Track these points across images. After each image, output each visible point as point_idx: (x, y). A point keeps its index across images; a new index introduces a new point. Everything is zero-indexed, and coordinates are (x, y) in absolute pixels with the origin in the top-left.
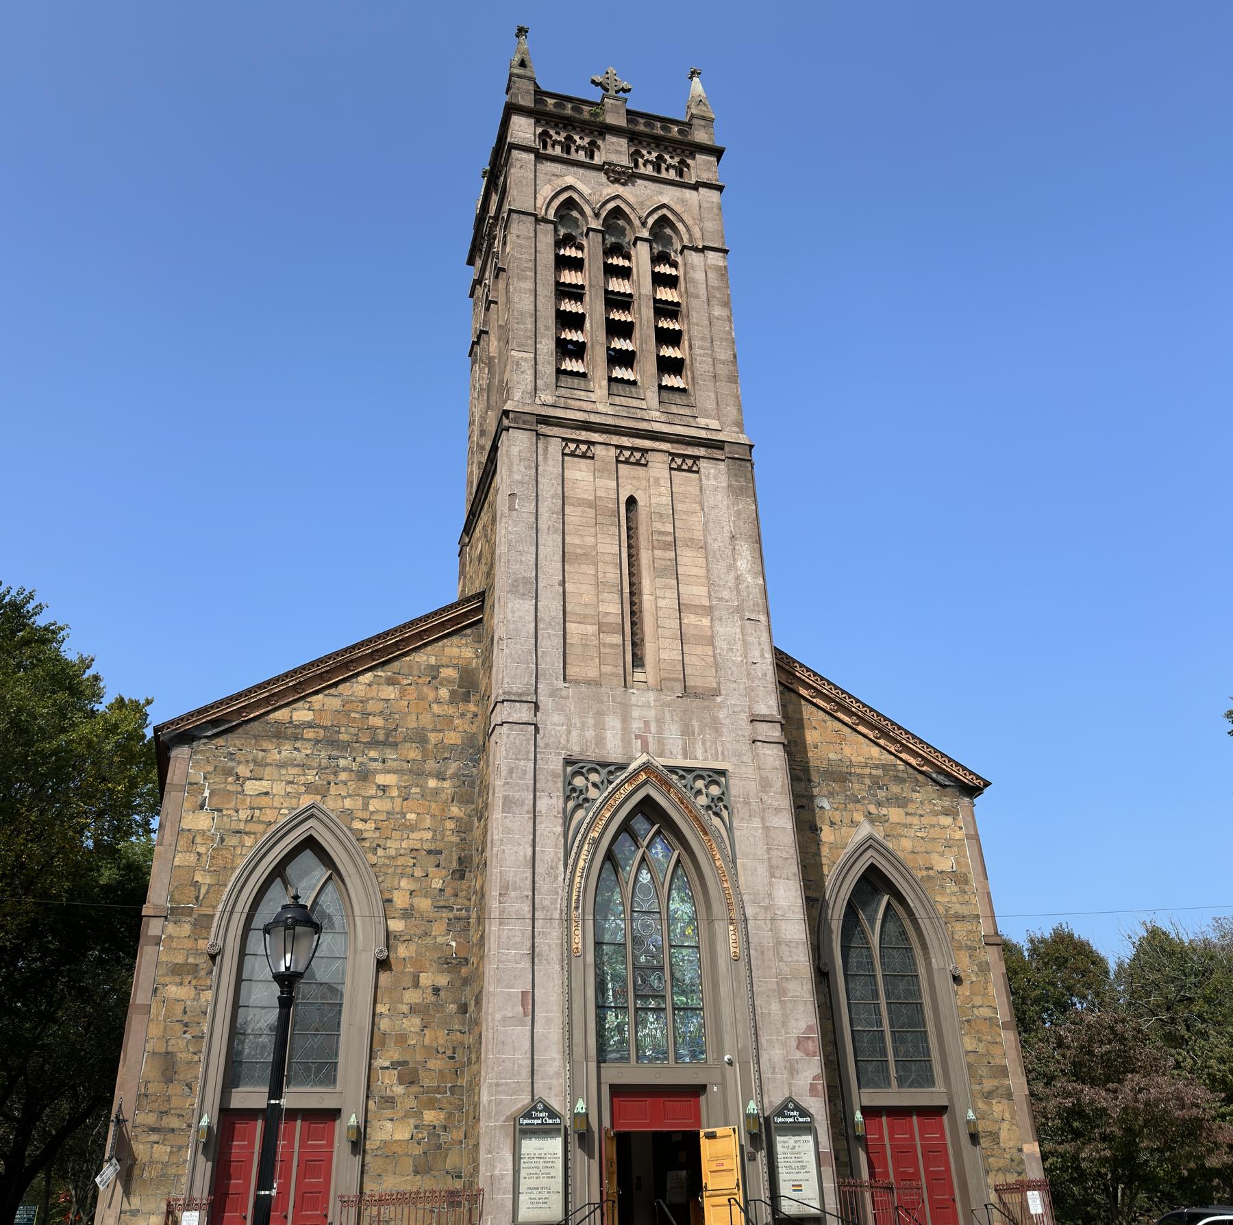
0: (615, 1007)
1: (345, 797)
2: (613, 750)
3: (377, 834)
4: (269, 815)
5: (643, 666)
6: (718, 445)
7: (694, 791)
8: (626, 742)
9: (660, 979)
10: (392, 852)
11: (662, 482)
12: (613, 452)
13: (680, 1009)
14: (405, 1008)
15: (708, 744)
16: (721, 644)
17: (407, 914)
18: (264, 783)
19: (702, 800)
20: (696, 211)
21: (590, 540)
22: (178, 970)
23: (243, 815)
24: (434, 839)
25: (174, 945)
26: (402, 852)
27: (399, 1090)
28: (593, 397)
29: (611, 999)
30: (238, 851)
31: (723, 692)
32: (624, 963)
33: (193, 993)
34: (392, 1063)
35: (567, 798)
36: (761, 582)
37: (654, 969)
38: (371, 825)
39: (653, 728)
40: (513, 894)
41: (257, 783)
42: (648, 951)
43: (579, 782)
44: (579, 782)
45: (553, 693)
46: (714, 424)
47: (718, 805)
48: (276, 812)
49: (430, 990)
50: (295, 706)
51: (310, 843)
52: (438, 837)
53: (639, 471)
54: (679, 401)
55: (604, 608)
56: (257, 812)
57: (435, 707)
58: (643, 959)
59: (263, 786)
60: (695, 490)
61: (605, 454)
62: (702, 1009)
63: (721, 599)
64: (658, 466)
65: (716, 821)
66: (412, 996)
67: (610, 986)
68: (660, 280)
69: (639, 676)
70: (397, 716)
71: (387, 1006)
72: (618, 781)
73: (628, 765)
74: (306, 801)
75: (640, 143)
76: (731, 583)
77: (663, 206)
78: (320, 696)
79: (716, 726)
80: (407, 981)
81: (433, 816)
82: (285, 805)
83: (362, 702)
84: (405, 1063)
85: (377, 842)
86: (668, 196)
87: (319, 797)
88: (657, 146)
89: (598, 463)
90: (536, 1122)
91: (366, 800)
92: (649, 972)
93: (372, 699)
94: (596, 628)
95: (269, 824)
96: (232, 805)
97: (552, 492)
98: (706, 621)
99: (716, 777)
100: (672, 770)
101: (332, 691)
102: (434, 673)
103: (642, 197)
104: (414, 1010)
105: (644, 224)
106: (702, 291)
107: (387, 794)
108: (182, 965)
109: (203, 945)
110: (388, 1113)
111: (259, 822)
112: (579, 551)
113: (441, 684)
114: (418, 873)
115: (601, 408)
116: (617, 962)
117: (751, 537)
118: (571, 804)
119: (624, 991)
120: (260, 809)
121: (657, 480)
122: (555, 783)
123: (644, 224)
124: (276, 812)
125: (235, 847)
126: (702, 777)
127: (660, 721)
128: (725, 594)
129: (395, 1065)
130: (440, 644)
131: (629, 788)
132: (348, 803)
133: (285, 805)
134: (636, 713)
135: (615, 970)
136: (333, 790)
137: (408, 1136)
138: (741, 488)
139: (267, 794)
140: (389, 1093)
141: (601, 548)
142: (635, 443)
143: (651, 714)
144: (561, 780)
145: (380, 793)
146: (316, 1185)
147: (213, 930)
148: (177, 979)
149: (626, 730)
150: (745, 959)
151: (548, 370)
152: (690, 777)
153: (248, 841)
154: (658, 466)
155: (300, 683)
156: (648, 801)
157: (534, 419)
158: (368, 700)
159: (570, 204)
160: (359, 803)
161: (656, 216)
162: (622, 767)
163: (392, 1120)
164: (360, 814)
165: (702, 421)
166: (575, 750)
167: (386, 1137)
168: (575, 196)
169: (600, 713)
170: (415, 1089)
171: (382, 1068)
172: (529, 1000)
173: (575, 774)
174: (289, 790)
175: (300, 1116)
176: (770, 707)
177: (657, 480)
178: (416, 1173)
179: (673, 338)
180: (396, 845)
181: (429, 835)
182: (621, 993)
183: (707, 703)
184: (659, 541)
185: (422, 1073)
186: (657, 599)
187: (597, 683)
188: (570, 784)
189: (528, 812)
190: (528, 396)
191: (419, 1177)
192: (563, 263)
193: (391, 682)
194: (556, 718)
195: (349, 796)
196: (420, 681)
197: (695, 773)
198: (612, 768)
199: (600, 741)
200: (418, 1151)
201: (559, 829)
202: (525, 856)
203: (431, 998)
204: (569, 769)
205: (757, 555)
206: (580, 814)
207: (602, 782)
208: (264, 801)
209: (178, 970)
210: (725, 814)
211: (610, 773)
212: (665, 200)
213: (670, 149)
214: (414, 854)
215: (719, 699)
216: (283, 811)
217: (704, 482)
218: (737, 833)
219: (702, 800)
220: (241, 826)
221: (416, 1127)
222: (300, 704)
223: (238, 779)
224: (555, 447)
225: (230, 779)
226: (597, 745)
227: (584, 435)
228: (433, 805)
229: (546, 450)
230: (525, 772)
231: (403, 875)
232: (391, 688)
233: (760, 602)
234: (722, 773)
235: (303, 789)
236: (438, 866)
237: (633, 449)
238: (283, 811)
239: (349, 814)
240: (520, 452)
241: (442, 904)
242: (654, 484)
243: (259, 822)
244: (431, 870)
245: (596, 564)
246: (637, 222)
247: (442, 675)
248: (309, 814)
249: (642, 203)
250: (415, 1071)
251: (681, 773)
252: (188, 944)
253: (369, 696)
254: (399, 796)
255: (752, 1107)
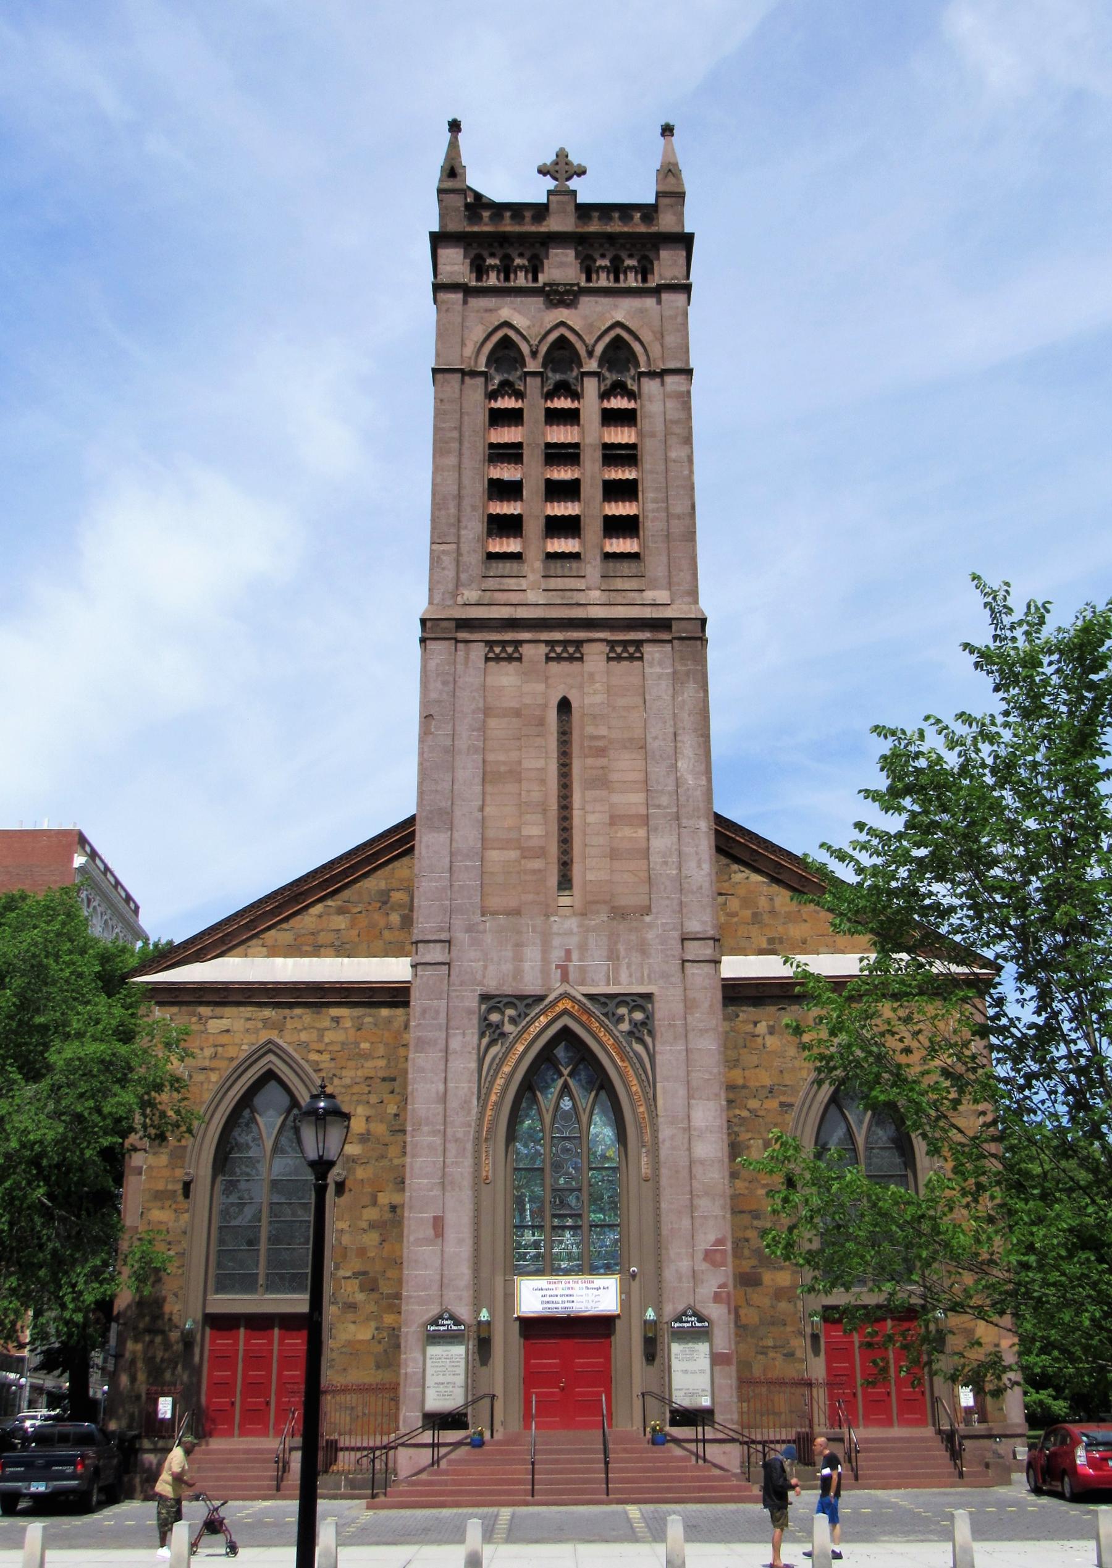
0: (533, 1227)
1: (301, 1030)
2: (531, 985)
3: (333, 1064)
4: (232, 1052)
5: (570, 888)
6: (664, 624)
7: (615, 1018)
8: (545, 973)
9: (578, 1198)
10: (348, 1081)
11: (597, 678)
12: (543, 649)
13: (597, 1226)
14: (364, 1225)
15: (633, 967)
16: (655, 859)
17: (364, 1138)
18: (224, 1021)
19: (625, 1026)
20: (657, 323)
21: (514, 755)
22: (159, 1196)
23: (208, 1052)
24: (388, 1066)
25: (154, 1174)
26: (358, 1080)
27: (360, 1297)
28: (524, 583)
29: (528, 1218)
30: (205, 1086)
31: (654, 910)
32: (543, 1185)
33: (173, 1216)
34: (354, 1274)
35: (482, 1035)
36: (704, 782)
37: (572, 1190)
38: (326, 1057)
39: (575, 956)
40: (425, 1129)
41: (218, 1021)
42: (568, 1174)
43: (495, 1017)
44: (495, 1017)
45: (470, 929)
46: (662, 596)
47: (643, 1031)
48: (237, 1048)
49: (387, 1208)
50: (250, 943)
51: (270, 1076)
52: (392, 1064)
53: (576, 665)
54: (626, 572)
55: (526, 831)
56: (220, 1049)
57: (386, 933)
58: (562, 1181)
59: (224, 1023)
60: (636, 680)
61: (534, 653)
62: (618, 1225)
63: (659, 806)
64: (595, 656)
65: (639, 1048)
66: (371, 1214)
67: (528, 1206)
68: (611, 418)
69: (565, 901)
70: (347, 946)
71: (348, 1223)
72: (532, 1015)
73: (546, 996)
74: (264, 1036)
75: (591, 245)
76: (671, 788)
77: (618, 324)
78: (273, 932)
79: (643, 949)
80: (366, 1200)
81: (386, 1044)
82: (245, 1041)
83: (313, 934)
84: (365, 1273)
85: (333, 1071)
86: (622, 310)
87: (276, 1032)
88: (612, 244)
89: (525, 663)
90: (442, 1328)
91: (321, 1032)
92: (567, 1193)
93: (322, 930)
94: (518, 852)
95: (232, 1059)
96: (197, 1043)
97: (473, 706)
98: (642, 832)
99: (640, 1001)
100: (591, 997)
101: (285, 926)
102: (384, 899)
103: (592, 318)
104: (373, 1226)
105: (590, 354)
106: (659, 427)
107: (341, 1025)
108: (162, 1192)
109: (179, 1173)
110: (350, 1316)
111: (222, 1058)
112: (503, 769)
113: (392, 909)
114: (374, 1099)
115: (532, 597)
116: (536, 1185)
117: (695, 730)
118: (485, 1041)
119: (541, 1210)
120: (222, 1046)
121: (591, 675)
122: (470, 1019)
123: (590, 354)
124: (237, 1048)
125: (202, 1083)
126: (626, 1003)
127: (583, 947)
128: (664, 800)
129: (356, 1275)
130: (390, 866)
131: (543, 1020)
132: (304, 1036)
133: (245, 1041)
134: (556, 941)
135: (532, 1192)
136: (290, 1024)
137: (369, 1337)
138: (687, 674)
139: (228, 1031)
140: (351, 1300)
141: (526, 764)
142: (567, 636)
143: (573, 942)
144: (476, 1016)
145: (335, 1025)
146: (293, 1376)
147: (187, 1159)
148: (159, 1204)
149: (545, 961)
150: (654, 1179)
151: (473, 559)
152: (612, 1004)
153: (214, 1077)
154: (595, 656)
155: (251, 921)
156: (566, 1031)
157: (453, 624)
158: (318, 932)
159: (506, 343)
160: (314, 1035)
161: (607, 339)
162: (540, 998)
163: (354, 1322)
164: (315, 1046)
165: (650, 595)
166: (492, 985)
167: (349, 1337)
168: (512, 334)
169: (519, 945)
170: (375, 1295)
171: (345, 1278)
172: (438, 1224)
173: (490, 1010)
174: (248, 1026)
175: (243, 1322)
176: (704, 923)
177: (591, 675)
178: (378, 1367)
179: (625, 490)
180: (352, 1073)
181: (382, 1063)
182: (538, 1213)
183: (634, 924)
184: (590, 747)
185: (381, 1283)
186: (588, 814)
187: (517, 912)
188: (486, 1019)
189: (441, 1051)
190: (447, 596)
191: (380, 1371)
192: (498, 418)
193: (341, 911)
194: (472, 954)
195: (305, 1029)
196: (370, 908)
197: (618, 1000)
198: (529, 1001)
199: (518, 973)
200: (379, 1349)
201: (473, 1065)
202: (437, 1093)
203: (388, 1216)
204: (484, 1007)
205: (701, 751)
206: (494, 1050)
207: (519, 1016)
208: (225, 1039)
209: (159, 1196)
210: (648, 1040)
211: (528, 1006)
212: (619, 317)
213: (628, 246)
214: (369, 1082)
215: (647, 919)
216: (244, 1047)
217: (648, 670)
218: (658, 1058)
219: (625, 1026)
220: (207, 1063)
221: (377, 1329)
222: (254, 942)
223: (200, 1019)
224: (478, 652)
225: (194, 1019)
226: (515, 978)
227: (508, 636)
228: (386, 1034)
229: (467, 658)
230: (437, 1012)
231: (359, 1102)
232: (341, 917)
233: (701, 805)
234: (648, 997)
235: (260, 1025)
236: (392, 1092)
237: (565, 643)
238: (244, 1047)
239: (304, 1046)
240: (438, 664)
241: (397, 1128)
242: (594, 680)
243: (222, 1058)
244: (386, 1097)
245: (520, 781)
246: (582, 352)
247: (392, 900)
248: (270, 1048)
249: (591, 325)
250: (375, 1281)
251: (603, 1000)
252: (166, 1173)
253: (320, 928)
254: (353, 1026)
255: (650, 1314)
